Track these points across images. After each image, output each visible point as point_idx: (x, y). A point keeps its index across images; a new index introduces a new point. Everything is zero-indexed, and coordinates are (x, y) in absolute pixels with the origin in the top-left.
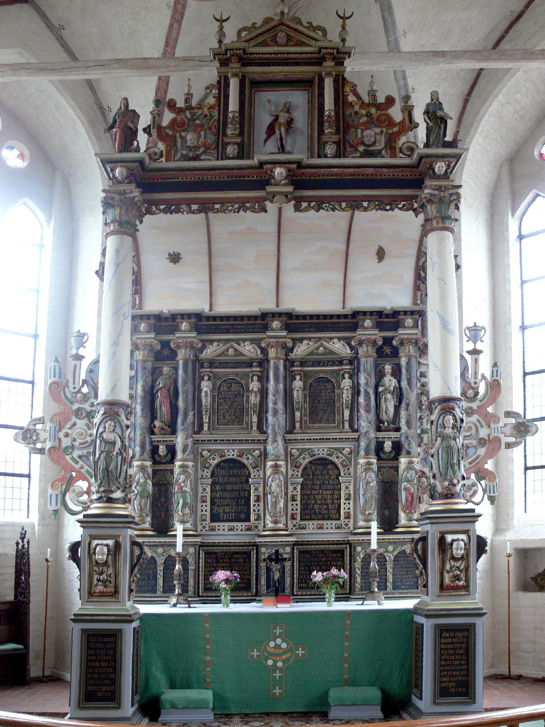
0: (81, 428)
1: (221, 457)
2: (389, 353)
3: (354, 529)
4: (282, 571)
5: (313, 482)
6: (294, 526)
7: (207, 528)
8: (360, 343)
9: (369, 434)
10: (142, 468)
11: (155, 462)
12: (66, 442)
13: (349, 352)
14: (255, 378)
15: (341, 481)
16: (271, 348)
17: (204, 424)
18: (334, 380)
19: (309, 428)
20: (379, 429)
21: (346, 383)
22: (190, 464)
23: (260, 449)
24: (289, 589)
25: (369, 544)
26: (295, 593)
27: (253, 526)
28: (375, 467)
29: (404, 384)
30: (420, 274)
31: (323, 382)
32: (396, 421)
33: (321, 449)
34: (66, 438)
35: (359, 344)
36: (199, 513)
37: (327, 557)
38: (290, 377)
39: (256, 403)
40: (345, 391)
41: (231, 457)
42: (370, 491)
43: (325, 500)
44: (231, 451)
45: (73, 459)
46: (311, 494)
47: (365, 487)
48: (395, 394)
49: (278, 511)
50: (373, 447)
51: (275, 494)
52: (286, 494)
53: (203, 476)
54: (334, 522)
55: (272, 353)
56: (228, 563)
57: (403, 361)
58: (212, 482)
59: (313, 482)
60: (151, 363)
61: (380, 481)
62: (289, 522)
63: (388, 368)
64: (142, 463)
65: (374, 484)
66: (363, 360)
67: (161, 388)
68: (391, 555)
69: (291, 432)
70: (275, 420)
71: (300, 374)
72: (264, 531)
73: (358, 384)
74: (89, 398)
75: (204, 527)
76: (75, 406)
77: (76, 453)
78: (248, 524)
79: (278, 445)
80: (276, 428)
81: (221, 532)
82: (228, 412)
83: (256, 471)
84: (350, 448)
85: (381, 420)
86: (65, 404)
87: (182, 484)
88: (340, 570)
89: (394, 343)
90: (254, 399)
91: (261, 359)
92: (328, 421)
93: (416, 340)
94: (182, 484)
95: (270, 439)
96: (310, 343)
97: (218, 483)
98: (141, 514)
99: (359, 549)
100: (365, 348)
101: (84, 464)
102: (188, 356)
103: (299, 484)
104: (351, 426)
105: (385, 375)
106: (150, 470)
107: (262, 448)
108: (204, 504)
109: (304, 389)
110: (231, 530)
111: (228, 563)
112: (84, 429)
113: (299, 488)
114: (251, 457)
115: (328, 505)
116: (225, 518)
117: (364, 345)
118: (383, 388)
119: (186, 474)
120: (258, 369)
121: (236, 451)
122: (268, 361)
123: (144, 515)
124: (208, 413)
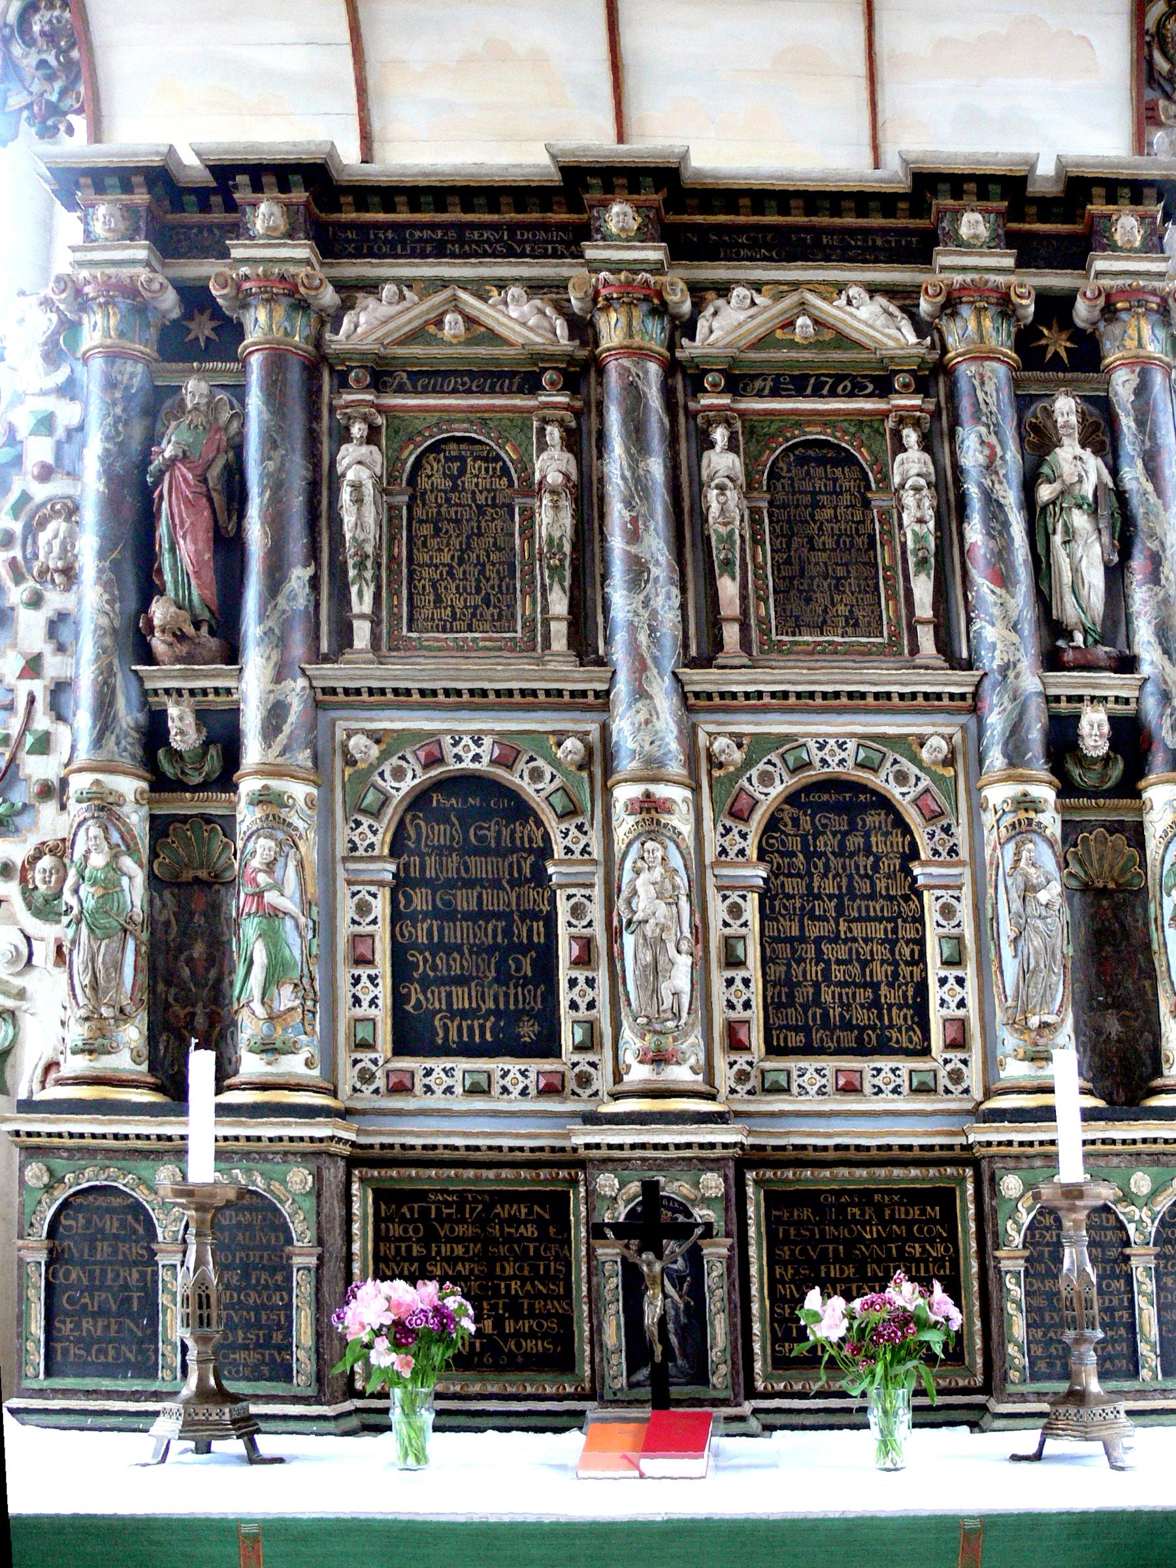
1: (426, 767)
2: (1063, 354)
3: (988, 1094)
4: (692, 1280)
5: (809, 887)
6: (742, 1077)
7: (380, 1082)
8: (950, 305)
9: (1017, 676)
11: (160, 784)
13: (912, 339)
14: (554, 433)
15: (921, 881)
16: (605, 309)
17: (356, 624)
18: (863, 456)
19: (780, 651)
20: (1052, 661)
21: (912, 464)
22: (299, 791)
23: (587, 733)
24: (723, 1369)
25: (1051, 1160)
26: (760, 1385)
27: (571, 1075)
28: (1051, 821)
29: (1133, 475)
30: (1150, 62)
31: (822, 462)
32: (1115, 632)
33: (832, 742)
35: (944, 307)
36: (346, 1013)
37: (882, 1222)
38: (687, 437)
39: (557, 535)
40: (909, 498)
41: (467, 764)
42: (1039, 923)
43: (864, 964)
44: (466, 740)
46: (802, 939)
47: (1017, 905)
48: (1103, 512)
49: (667, 1005)
50: (1035, 733)
51: (649, 929)
52: (700, 932)
53: (354, 848)
54: (906, 1065)
55: (612, 330)
56: (475, 1239)
57: (1123, 385)
58: (395, 876)
59: (809, 887)
60: (140, 368)
61: (1074, 884)
62: (720, 1062)
63: (1065, 408)
65: (1052, 893)
66: (966, 371)
67: (172, 463)
68: (1145, 1214)
69: (704, 661)
70: (641, 607)
71: (728, 423)
72: (616, 1097)
73: (957, 469)
75: (366, 1077)
78: (548, 1065)
79: (653, 712)
80: (643, 638)
81: (437, 1101)
82: (450, 573)
83: (573, 831)
84: (949, 738)
85: (1059, 623)
87: (262, 879)
88: (925, 1284)
89: (1082, 311)
90: (553, 521)
91: (571, 359)
92: (852, 624)
93: (1164, 300)
94: (262, 879)
95: (622, 688)
96: (758, 299)
97: (423, 882)
98: (96, 1010)
99: (1011, 1185)
100: (972, 325)
102: (279, 335)
103: (751, 889)
104: (945, 645)
105: (1059, 444)
106: (136, 819)
107: (594, 728)
108: (364, 972)
109: (750, 486)
110: (474, 1090)
111: (475, 1239)
113: (751, 908)
114: (548, 770)
115: (876, 986)
116: (453, 1035)
117: (966, 311)
118: (1057, 486)
119: (280, 835)
120: (562, 399)
121: (487, 741)
122: (601, 371)
123: (105, 1011)
124: (368, 575)
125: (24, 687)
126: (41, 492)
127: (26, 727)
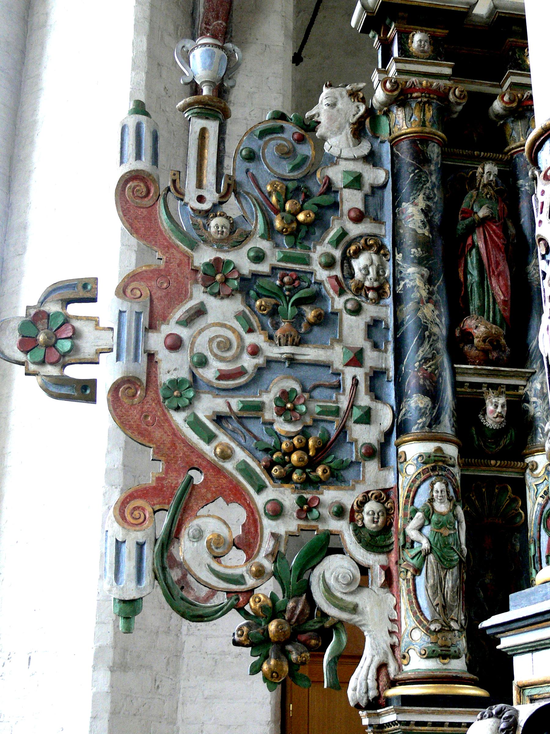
0: (224, 326)
10: (434, 465)
12: (173, 367)
34: (174, 355)
45: (196, 424)
64: (439, 449)
74: (247, 236)
76: (204, 256)
77: (207, 406)
86: (168, 247)
101: (233, 445)
112: (234, 330)
125: (350, 372)
126: (354, 230)
127: (352, 405)
